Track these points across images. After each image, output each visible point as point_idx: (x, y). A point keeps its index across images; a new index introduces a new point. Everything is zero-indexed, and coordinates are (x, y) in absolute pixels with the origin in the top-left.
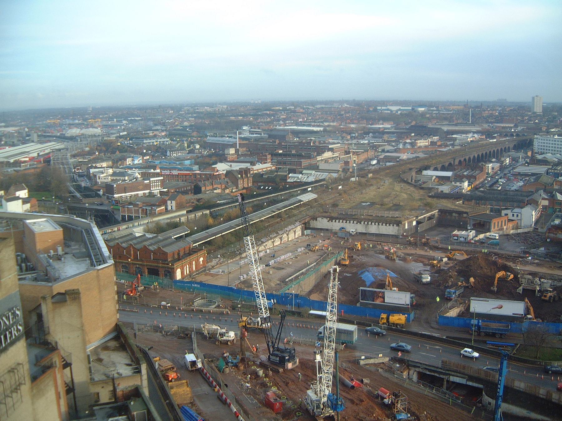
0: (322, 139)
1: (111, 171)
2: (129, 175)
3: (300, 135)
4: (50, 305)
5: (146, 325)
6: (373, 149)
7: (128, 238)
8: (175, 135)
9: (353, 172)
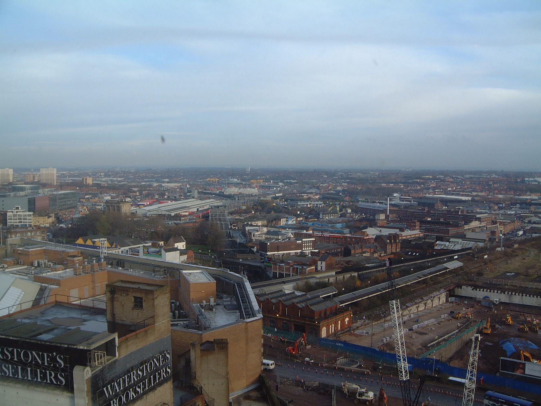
0: (470, 209)
1: (265, 230)
2: (283, 235)
3: (449, 204)
4: (198, 351)
5: (288, 379)
6: (519, 220)
7: (278, 294)
8: (328, 198)
9: (499, 242)
